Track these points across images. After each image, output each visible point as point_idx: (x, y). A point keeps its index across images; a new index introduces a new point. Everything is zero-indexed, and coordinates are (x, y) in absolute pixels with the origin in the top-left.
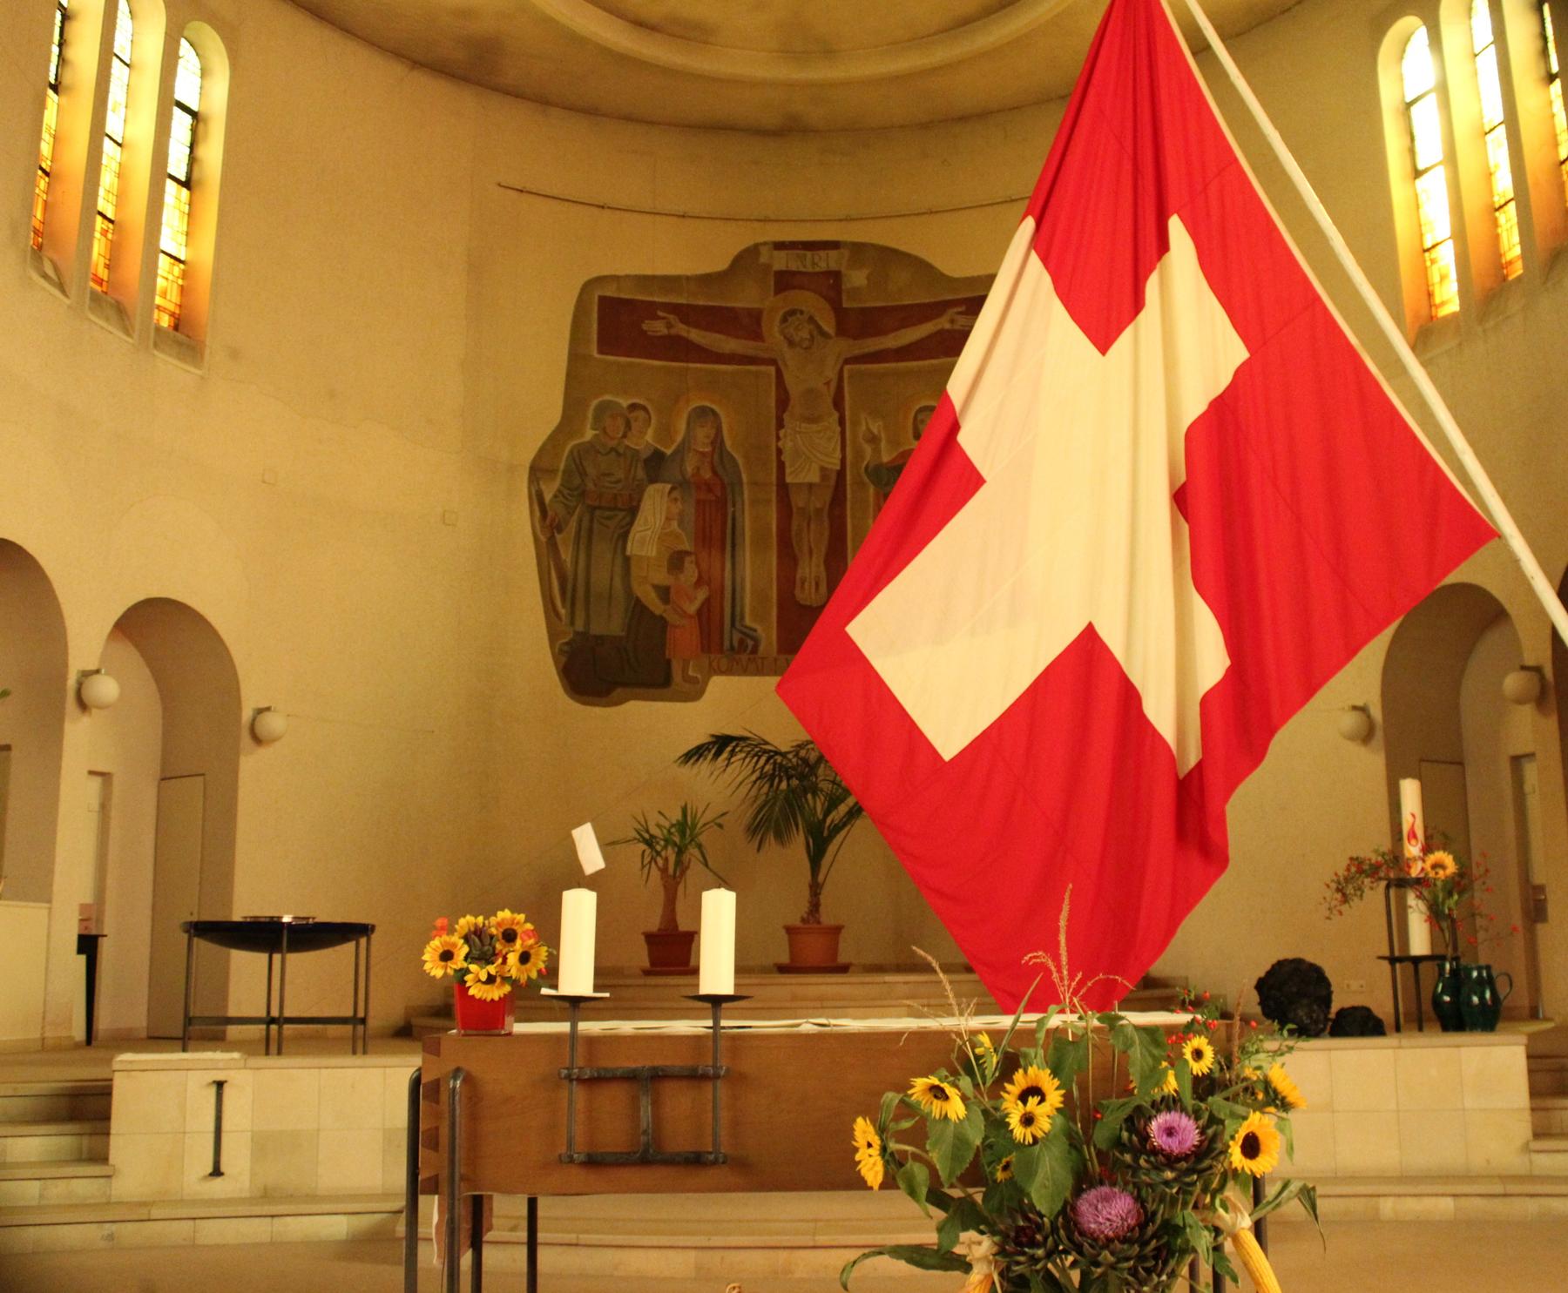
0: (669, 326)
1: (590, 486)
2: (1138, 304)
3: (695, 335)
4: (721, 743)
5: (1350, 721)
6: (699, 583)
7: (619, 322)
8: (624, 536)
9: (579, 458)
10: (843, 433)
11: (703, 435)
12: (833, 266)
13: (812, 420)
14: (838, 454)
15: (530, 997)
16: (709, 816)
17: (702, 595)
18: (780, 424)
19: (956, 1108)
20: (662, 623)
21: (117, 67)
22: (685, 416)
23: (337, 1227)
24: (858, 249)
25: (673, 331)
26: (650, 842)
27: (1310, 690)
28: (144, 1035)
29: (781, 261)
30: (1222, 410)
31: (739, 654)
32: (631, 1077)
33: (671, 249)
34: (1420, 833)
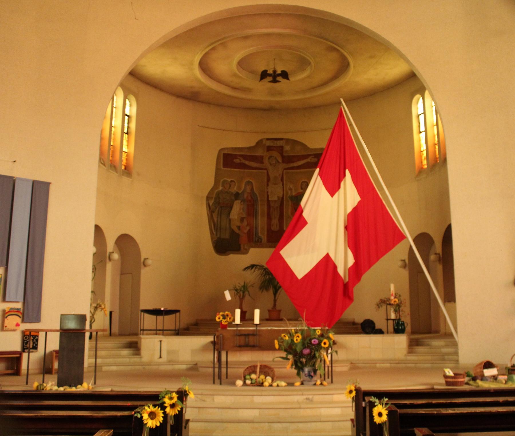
0: (240, 160)
1: (221, 201)
2: (339, 187)
3: (247, 163)
4: (252, 266)
5: (400, 263)
6: (248, 225)
7: (228, 159)
8: (229, 214)
9: (218, 197)
10: (283, 188)
11: (248, 190)
12: (281, 145)
13: (275, 184)
14: (282, 193)
15: (231, 324)
16: (249, 285)
17: (248, 228)
18: (268, 185)
19: (287, 338)
20: (238, 235)
21: (114, 109)
22: (244, 183)
23: (184, 367)
24: (288, 141)
25: (241, 162)
26: (236, 290)
27: (370, 267)
28: (117, 334)
29: (268, 143)
30: (355, 210)
31: (257, 243)
32: (245, 335)
33: (240, 140)
34: (394, 294)
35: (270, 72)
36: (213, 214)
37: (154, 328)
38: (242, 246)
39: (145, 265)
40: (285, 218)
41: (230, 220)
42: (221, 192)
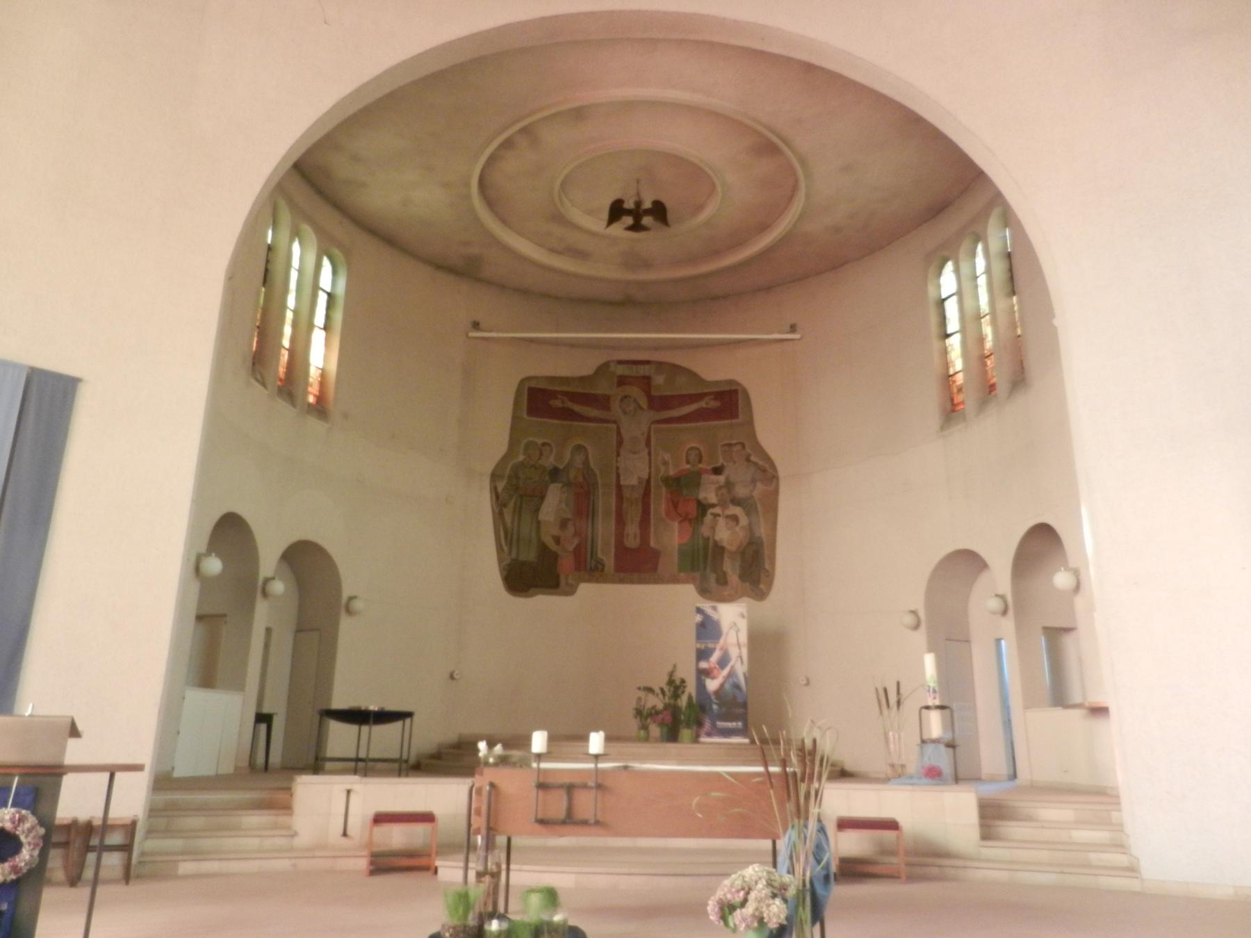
3: (577, 408)
6: (576, 534)
7: (539, 400)
8: (537, 510)
9: (515, 474)
11: (579, 459)
12: (647, 374)
17: (576, 541)
18: (618, 455)
20: (555, 556)
29: (621, 370)
36: (505, 510)
37: (353, 755)
39: (349, 611)
40: (652, 521)
41: (539, 523)
42: (522, 464)
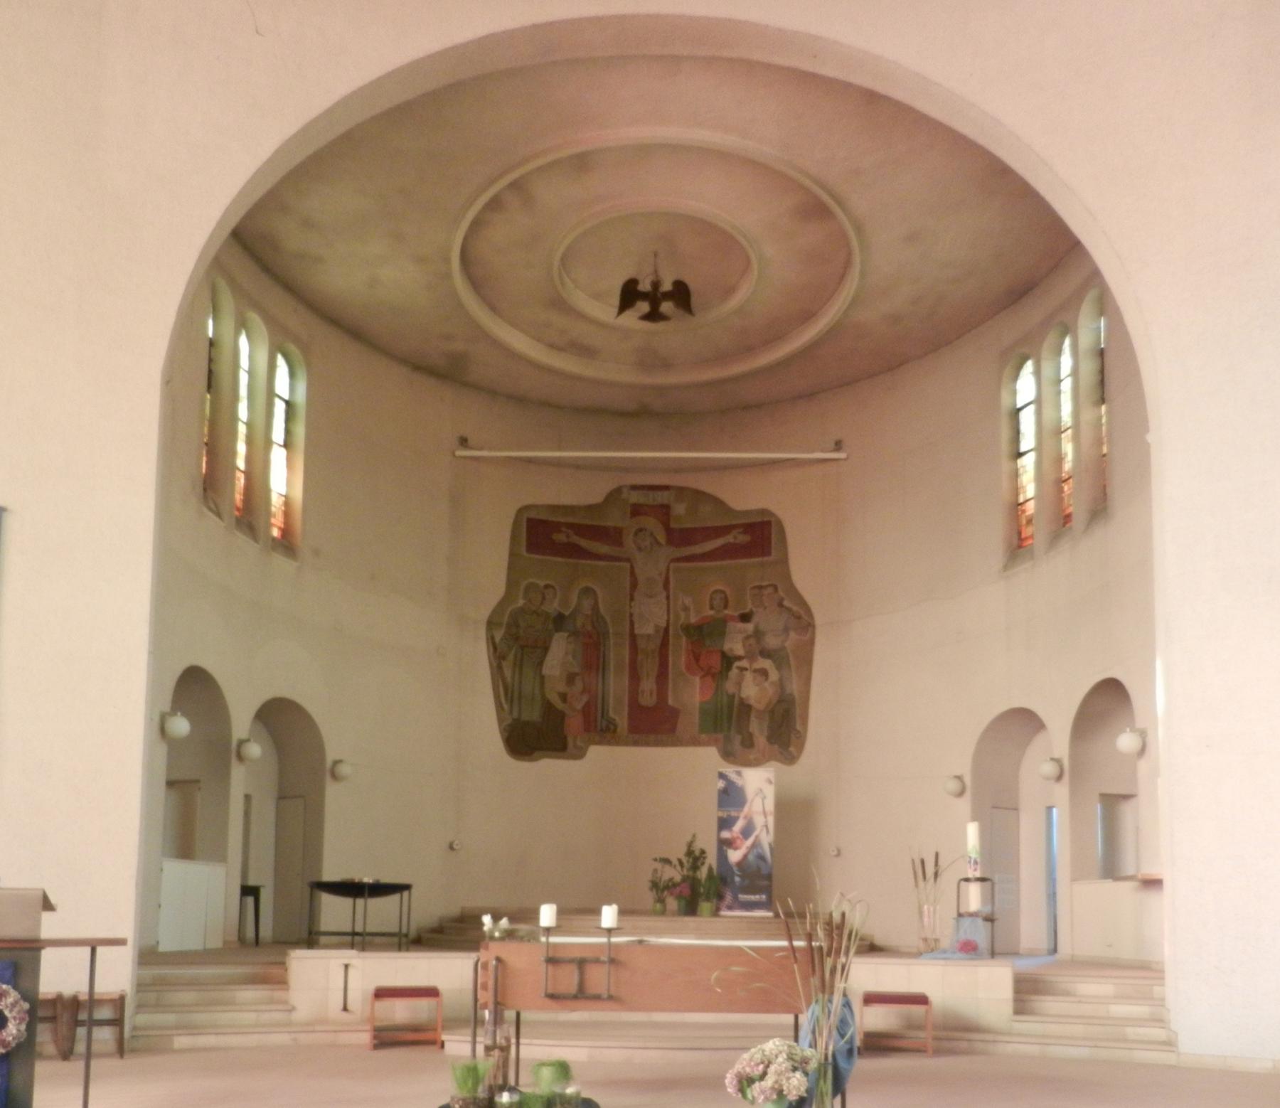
0: (568, 536)
3: (584, 543)
6: (583, 692)
7: (541, 534)
8: (540, 664)
9: (514, 623)
11: (587, 604)
12: (666, 502)
17: (585, 699)
18: (632, 599)
20: (562, 716)
24: (681, 491)
29: (635, 497)
35: (645, 286)
36: (504, 664)
37: (349, 929)
38: (570, 740)
39: (335, 776)
40: (670, 676)
41: (542, 677)
42: (522, 610)
